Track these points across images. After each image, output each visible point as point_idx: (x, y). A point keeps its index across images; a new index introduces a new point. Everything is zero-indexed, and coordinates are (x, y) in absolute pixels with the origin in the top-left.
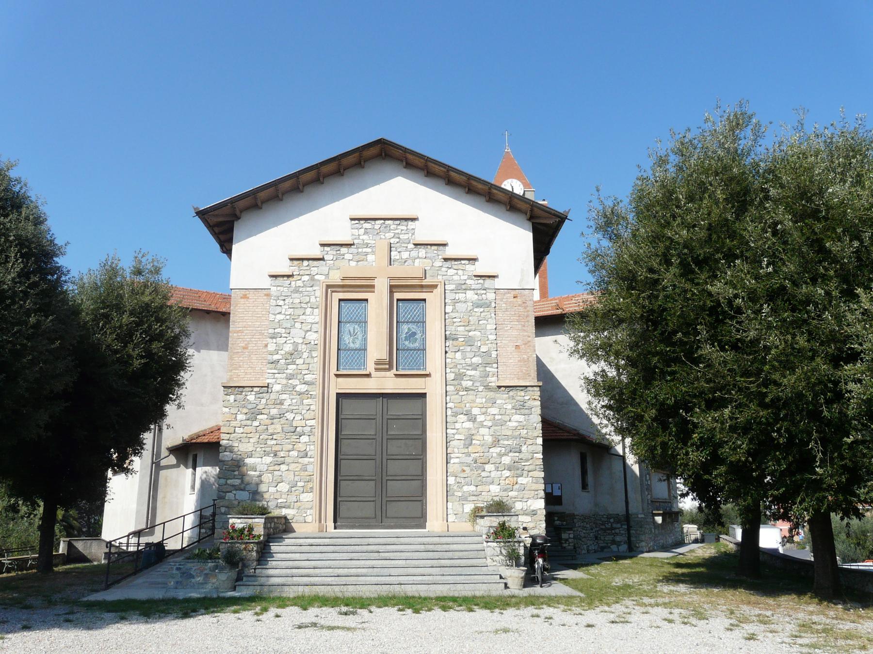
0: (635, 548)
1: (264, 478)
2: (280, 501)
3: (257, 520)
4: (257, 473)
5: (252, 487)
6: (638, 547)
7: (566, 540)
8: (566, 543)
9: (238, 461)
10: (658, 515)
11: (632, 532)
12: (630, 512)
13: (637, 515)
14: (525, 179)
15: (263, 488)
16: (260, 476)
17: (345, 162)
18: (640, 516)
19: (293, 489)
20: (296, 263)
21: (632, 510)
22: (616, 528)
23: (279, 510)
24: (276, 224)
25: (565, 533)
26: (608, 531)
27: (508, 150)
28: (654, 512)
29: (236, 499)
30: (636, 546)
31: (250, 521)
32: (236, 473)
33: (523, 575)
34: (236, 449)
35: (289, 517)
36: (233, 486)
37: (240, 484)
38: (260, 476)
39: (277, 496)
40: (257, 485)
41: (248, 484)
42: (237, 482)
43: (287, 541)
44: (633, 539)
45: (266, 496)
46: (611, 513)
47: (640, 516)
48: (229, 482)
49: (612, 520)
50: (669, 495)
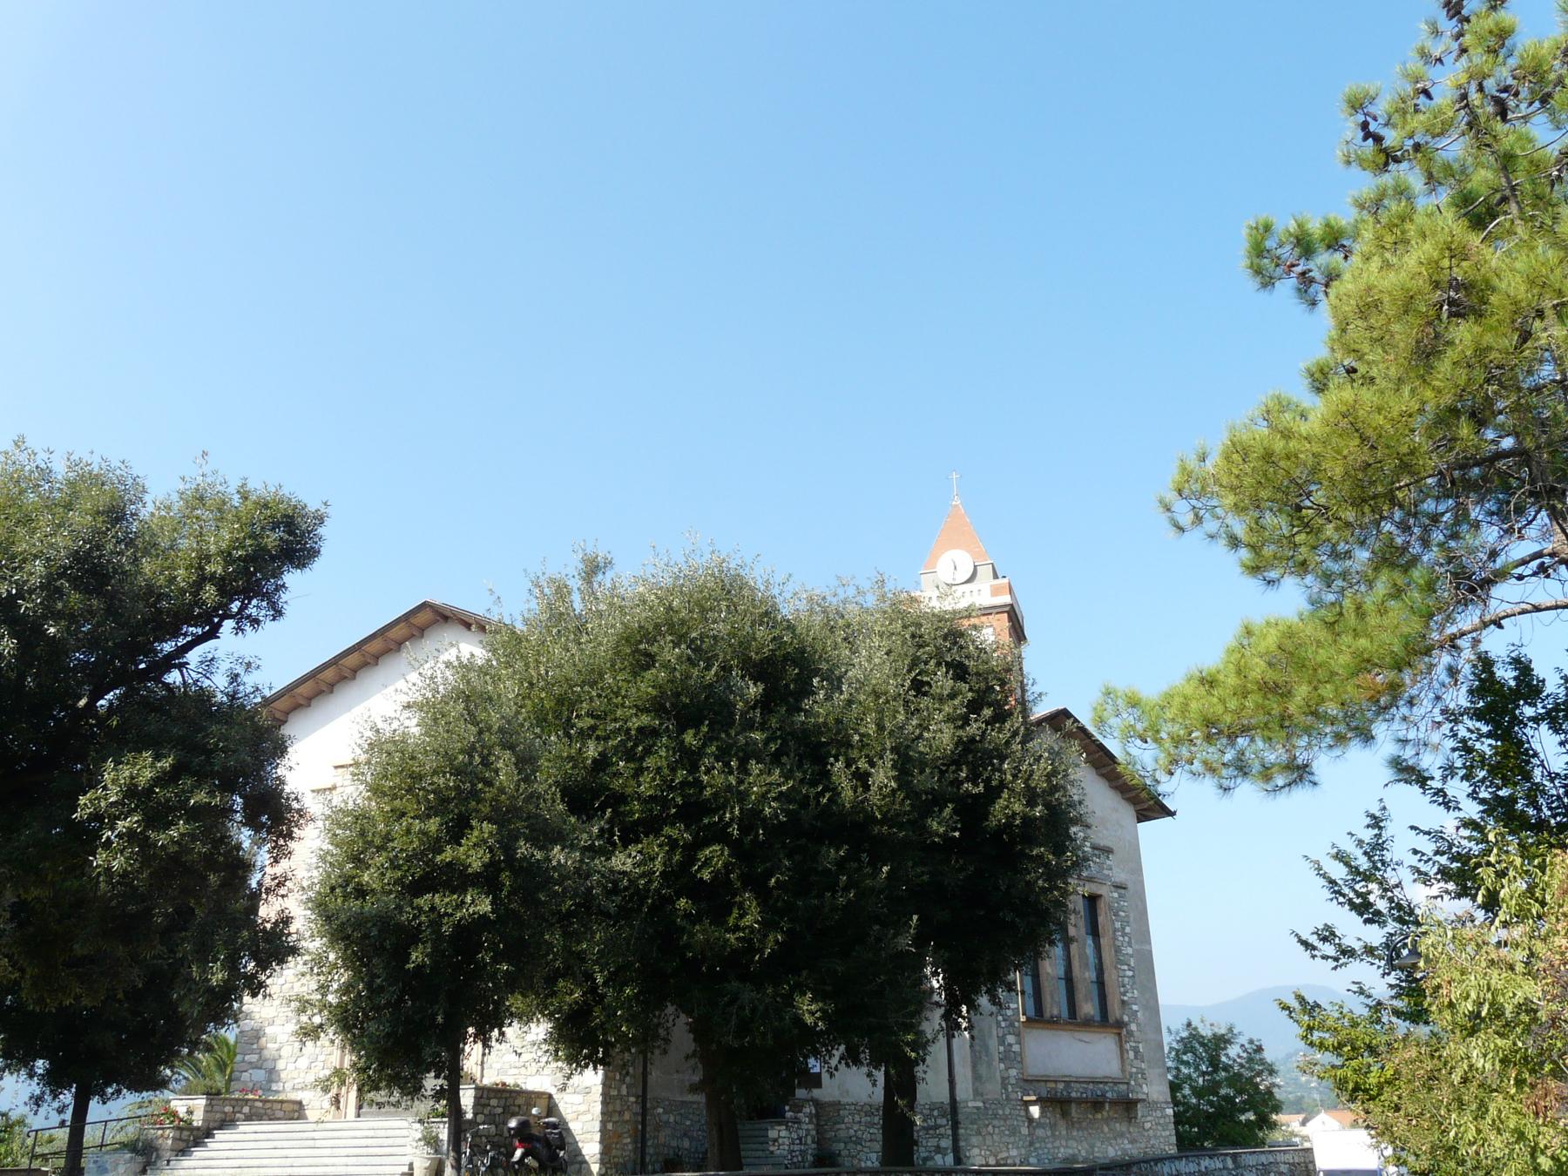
0: (964, 1160)
1: (283, 1053)
2: (296, 1081)
3: (196, 1102)
4: (276, 1046)
5: (269, 1065)
6: (969, 1158)
7: (775, 1140)
8: (774, 1145)
9: (258, 1031)
10: (1033, 1103)
11: (961, 1131)
12: (958, 1099)
13: (967, 1102)
14: (979, 547)
15: (280, 1065)
16: (279, 1049)
17: (395, 634)
18: (970, 1104)
19: (313, 1065)
20: (340, 770)
21: (960, 1095)
22: (941, 1126)
23: (295, 1094)
24: (323, 725)
25: (773, 1129)
26: (931, 1132)
27: (957, 502)
28: (1025, 1098)
29: (251, 1081)
30: (966, 1156)
31: (190, 1102)
32: (255, 1046)
33: (428, 1165)
34: (257, 1016)
35: (304, 1103)
36: (250, 1063)
37: (258, 1061)
38: (279, 1049)
39: (295, 1074)
40: (275, 1060)
41: (266, 1060)
42: (253, 1058)
43: (241, 1128)
44: (962, 1144)
45: (283, 1075)
46: (935, 1101)
47: (970, 1104)
48: (247, 1058)
49: (936, 1113)
50: (1123, 1071)
